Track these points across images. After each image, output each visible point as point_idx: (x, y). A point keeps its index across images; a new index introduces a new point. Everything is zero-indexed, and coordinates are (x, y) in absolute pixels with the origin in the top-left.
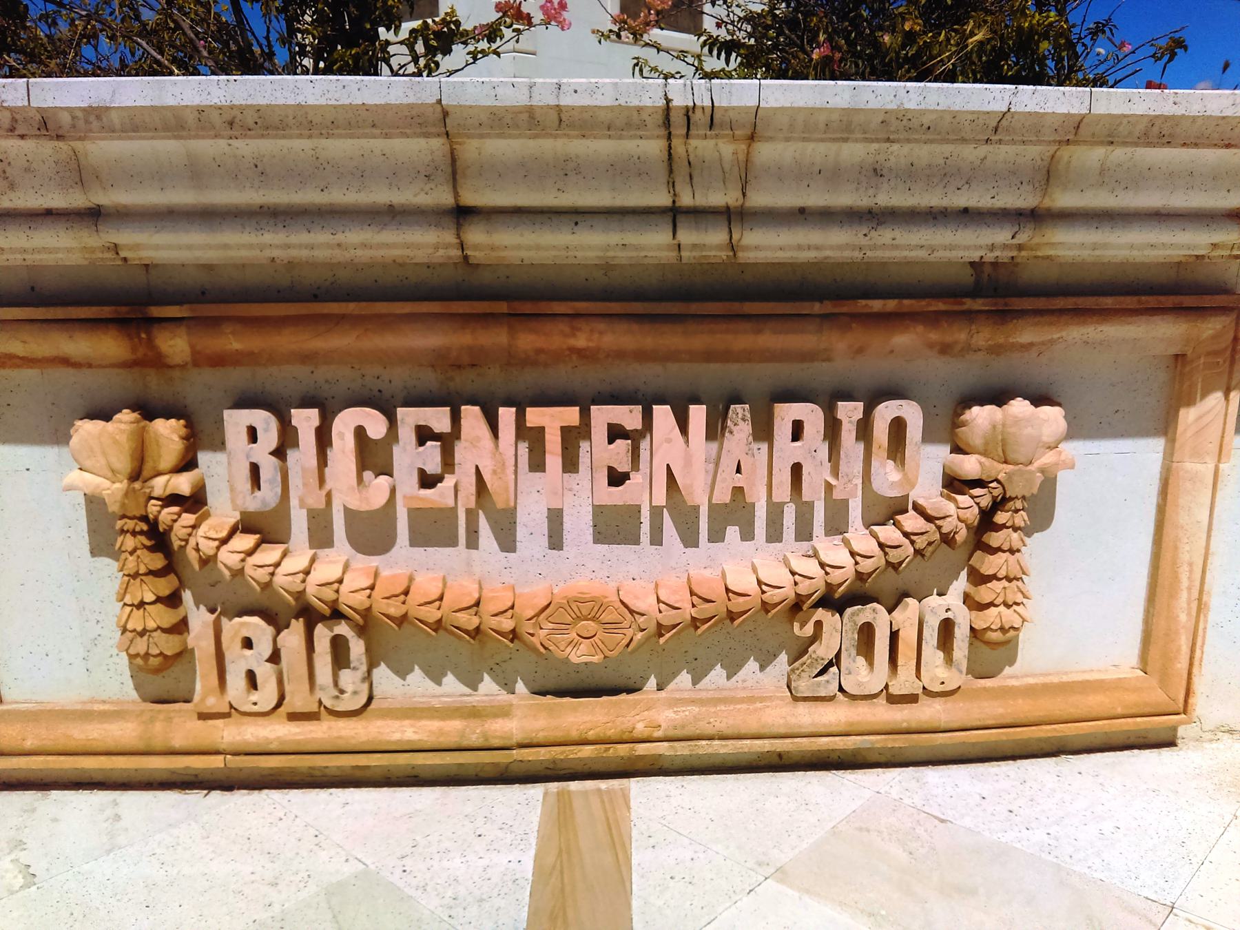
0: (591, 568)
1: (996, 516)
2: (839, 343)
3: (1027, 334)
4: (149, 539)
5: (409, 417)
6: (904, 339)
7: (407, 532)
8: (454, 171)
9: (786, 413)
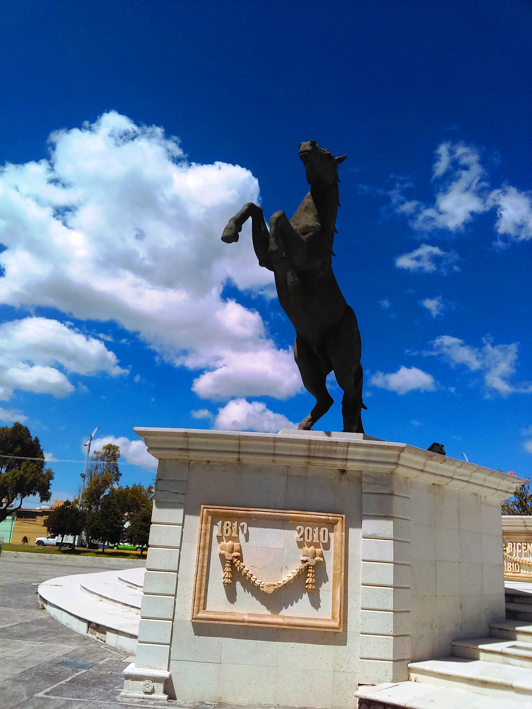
5: (523, 544)
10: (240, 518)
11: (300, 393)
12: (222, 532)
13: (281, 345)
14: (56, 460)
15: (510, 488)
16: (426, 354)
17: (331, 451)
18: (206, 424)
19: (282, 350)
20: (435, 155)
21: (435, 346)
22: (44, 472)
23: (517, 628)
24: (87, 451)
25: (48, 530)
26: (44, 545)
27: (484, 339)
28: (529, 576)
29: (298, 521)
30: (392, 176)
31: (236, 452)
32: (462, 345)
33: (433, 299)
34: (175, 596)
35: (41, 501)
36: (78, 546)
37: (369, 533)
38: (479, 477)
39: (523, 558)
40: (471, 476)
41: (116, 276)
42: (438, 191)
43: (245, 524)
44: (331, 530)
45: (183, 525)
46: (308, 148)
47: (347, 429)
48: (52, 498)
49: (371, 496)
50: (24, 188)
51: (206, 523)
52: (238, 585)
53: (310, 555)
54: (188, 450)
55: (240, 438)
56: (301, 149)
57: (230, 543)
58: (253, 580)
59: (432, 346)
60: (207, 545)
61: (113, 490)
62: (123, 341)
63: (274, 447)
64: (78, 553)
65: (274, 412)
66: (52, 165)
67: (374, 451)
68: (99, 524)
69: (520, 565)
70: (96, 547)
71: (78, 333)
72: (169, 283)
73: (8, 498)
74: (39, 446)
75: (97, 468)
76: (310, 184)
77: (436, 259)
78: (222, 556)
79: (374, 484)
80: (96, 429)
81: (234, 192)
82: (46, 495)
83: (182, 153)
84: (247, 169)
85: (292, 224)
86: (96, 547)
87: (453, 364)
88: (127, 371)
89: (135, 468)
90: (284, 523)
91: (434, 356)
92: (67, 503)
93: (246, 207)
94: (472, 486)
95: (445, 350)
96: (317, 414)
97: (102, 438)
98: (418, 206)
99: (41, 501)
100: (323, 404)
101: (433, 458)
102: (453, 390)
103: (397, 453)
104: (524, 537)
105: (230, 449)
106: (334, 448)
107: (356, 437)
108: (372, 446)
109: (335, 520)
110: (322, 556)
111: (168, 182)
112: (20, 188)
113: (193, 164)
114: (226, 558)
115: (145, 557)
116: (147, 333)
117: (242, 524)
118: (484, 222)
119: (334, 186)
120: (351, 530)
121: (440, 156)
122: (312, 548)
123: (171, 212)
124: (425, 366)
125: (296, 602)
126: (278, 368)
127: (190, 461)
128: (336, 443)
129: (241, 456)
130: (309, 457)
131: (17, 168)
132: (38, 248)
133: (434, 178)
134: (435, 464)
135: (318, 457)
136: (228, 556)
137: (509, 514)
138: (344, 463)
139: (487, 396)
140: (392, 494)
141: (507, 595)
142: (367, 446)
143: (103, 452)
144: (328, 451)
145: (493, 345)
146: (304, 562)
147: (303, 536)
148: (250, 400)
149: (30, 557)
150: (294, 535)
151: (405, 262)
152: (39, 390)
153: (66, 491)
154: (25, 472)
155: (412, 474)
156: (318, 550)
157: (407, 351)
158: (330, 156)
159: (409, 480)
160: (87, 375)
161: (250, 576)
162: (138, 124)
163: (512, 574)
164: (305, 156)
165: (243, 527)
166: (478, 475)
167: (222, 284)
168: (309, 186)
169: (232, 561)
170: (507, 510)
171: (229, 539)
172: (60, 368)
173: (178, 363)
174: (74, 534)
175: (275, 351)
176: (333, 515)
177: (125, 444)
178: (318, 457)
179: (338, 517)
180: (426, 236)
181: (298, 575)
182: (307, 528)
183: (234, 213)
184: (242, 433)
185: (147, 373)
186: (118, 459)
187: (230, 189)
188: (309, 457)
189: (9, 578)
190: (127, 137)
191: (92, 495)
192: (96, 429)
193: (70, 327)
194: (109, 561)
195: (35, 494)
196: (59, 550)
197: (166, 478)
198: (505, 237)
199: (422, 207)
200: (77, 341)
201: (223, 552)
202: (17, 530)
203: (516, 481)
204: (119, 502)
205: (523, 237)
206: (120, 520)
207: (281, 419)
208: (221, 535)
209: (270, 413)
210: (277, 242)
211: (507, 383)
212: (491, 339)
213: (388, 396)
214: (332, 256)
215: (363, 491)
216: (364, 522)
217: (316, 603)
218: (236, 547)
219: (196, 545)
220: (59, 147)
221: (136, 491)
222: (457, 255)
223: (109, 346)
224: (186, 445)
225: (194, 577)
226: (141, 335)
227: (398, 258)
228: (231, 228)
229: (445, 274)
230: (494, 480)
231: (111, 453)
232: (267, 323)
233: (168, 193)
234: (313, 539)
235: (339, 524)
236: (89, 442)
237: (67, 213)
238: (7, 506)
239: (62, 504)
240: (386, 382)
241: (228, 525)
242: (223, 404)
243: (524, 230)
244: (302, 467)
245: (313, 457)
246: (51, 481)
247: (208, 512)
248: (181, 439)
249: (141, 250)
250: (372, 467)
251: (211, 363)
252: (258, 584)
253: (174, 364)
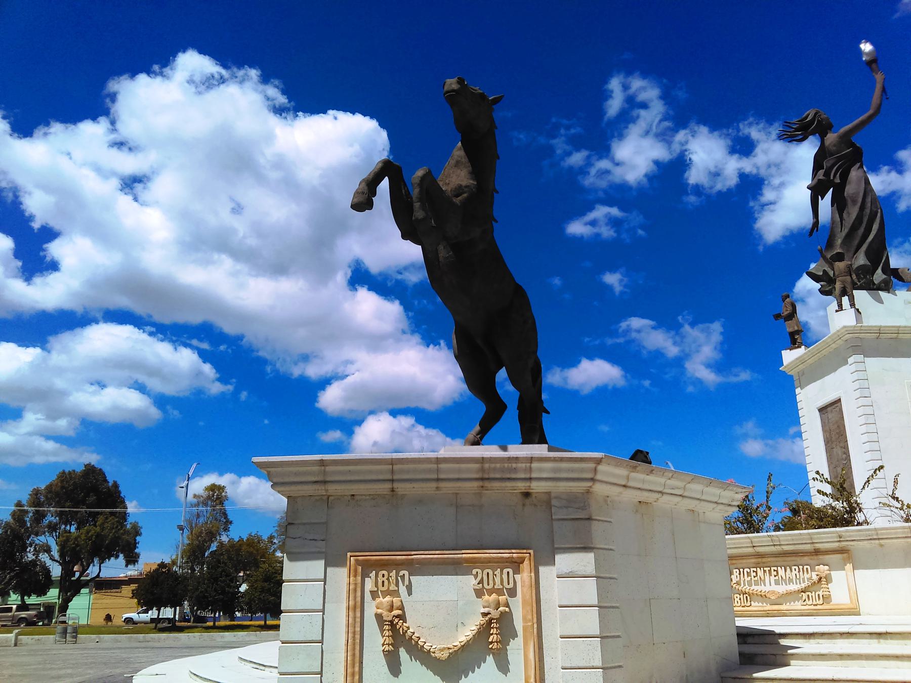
3: (821, 557)
4: (571, 168)
6: (806, 558)
7: (829, 676)
9: (793, 568)
11: (457, 400)
12: (376, 586)
13: (429, 340)
14: (143, 510)
15: (733, 500)
16: (609, 341)
18: (338, 447)
20: (606, 90)
21: (620, 330)
22: (128, 527)
23: (755, 675)
24: (184, 494)
25: (139, 603)
26: (135, 623)
27: (680, 318)
28: (762, 609)
29: (474, 562)
30: (554, 120)
31: (389, 480)
32: (654, 328)
33: (615, 273)
34: (321, 673)
35: (127, 566)
36: (180, 621)
37: (565, 570)
38: (696, 488)
39: (753, 587)
40: (684, 488)
41: (207, 263)
42: (613, 137)
43: (406, 573)
44: (517, 571)
45: (325, 580)
46: (455, 86)
47: (527, 439)
48: (141, 560)
50: (77, 154)
52: (403, 652)
53: (493, 606)
55: (392, 462)
56: (446, 88)
57: (388, 598)
58: (421, 644)
59: (617, 330)
60: (359, 604)
61: (221, 543)
62: (222, 348)
64: (181, 630)
65: (426, 427)
66: (113, 123)
67: (564, 465)
68: (206, 590)
70: (203, 620)
71: (162, 341)
73: (82, 565)
74: (120, 492)
75: (198, 516)
77: (614, 223)
78: (379, 617)
79: (567, 507)
80: (194, 466)
81: (357, 148)
82: (132, 557)
83: (287, 101)
84: (371, 118)
85: (441, 184)
86: (203, 620)
87: (645, 352)
88: (230, 388)
89: (250, 513)
91: (620, 344)
92: (162, 565)
95: (634, 335)
97: (202, 476)
98: (588, 157)
99: (127, 566)
102: (647, 383)
104: (753, 560)
105: (381, 477)
106: (514, 465)
107: (539, 450)
108: (562, 460)
110: (507, 605)
111: (270, 138)
112: (74, 155)
113: (300, 114)
115: (276, 627)
116: (253, 335)
118: (673, 170)
120: (542, 569)
121: (612, 92)
123: (274, 175)
125: (479, 668)
126: (434, 372)
127: (329, 496)
128: (517, 459)
129: (396, 485)
130: (482, 479)
131: (67, 128)
132: (102, 232)
133: (606, 119)
134: (640, 476)
136: (387, 616)
137: (732, 533)
138: (528, 484)
139: (690, 389)
140: (589, 519)
141: (738, 635)
142: (555, 460)
143: (205, 494)
145: (693, 324)
146: (485, 615)
147: (481, 582)
148: (394, 413)
149: (117, 641)
150: (469, 582)
151: (576, 228)
152: (115, 418)
153: (158, 550)
154: (103, 529)
157: (587, 339)
158: (483, 97)
160: (177, 395)
161: (416, 639)
162: (225, 66)
163: (741, 608)
164: (452, 98)
166: (693, 486)
167: (350, 267)
169: (392, 622)
171: (386, 593)
172: (141, 388)
173: (296, 372)
174: (173, 606)
175: (423, 348)
177: (233, 483)
179: (527, 555)
180: (601, 194)
181: (479, 633)
183: (367, 172)
185: (255, 388)
186: (226, 503)
187: (351, 145)
188: (482, 479)
189: (91, 672)
190: (210, 83)
191: (194, 553)
192: (194, 466)
193: (151, 334)
194: (222, 637)
195: (117, 557)
196: (155, 628)
198: (698, 190)
200: (162, 352)
201: (379, 611)
202: (97, 606)
203: (740, 490)
204: (230, 559)
205: (719, 186)
206: (234, 582)
207: (437, 436)
209: (421, 429)
210: (423, 207)
211: (712, 372)
212: (690, 318)
213: (572, 396)
216: (558, 558)
217: (503, 666)
218: (396, 600)
219: (344, 605)
220: (120, 97)
221: (253, 543)
222: (641, 217)
223: (204, 356)
224: (323, 475)
225: (344, 647)
226: (245, 340)
227: (568, 223)
228: (363, 193)
229: (628, 241)
230: (713, 492)
231: (216, 495)
232: (410, 314)
233: (269, 152)
234: (494, 584)
235: (526, 562)
236: (186, 482)
237: (136, 185)
238: (81, 575)
239: (155, 567)
240: (565, 379)
241: (383, 576)
242: (360, 422)
243: (719, 178)
244: (475, 494)
245: (488, 479)
246: (138, 538)
247: (356, 560)
248: (316, 468)
249: (240, 227)
250: (563, 487)
251: (340, 370)
252: (428, 648)
253: (292, 374)
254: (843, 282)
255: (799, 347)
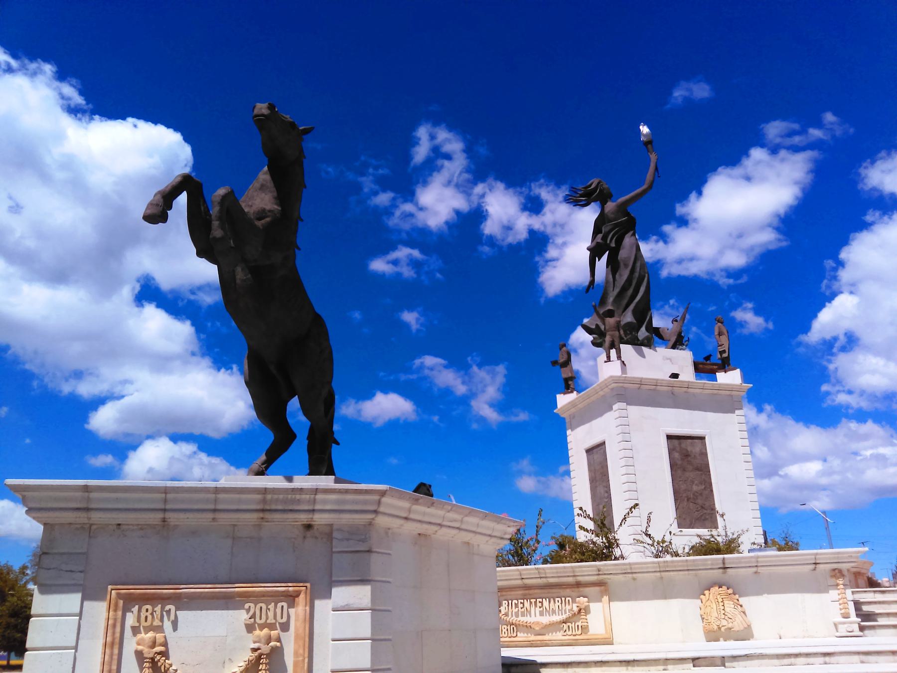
0: (539, 619)
1: (583, 611)
2: (561, 591)
3: (581, 589)
8: (574, 572)
10: (164, 600)
12: (139, 620)
13: (220, 363)
15: (505, 533)
16: (403, 377)
17: (294, 501)
19: (223, 370)
21: (415, 367)
29: (247, 597)
32: (446, 367)
38: (472, 521)
40: (462, 521)
42: (418, 182)
44: (292, 605)
46: (266, 111)
47: (314, 471)
49: (345, 555)
51: (115, 610)
53: (263, 640)
54: (87, 510)
56: (256, 112)
57: (151, 634)
60: (117, 640)
63: (214, 500)
65: (209, 455)
69: (516, 627)
72: (57, 276)
76: (267, 156)
77: (415, 264)
78: (139, 655)
79: (348, 540)
81: (156, 160)
85: (243, 205)
90: (228, 602)
93: (179, 179)
94: (463, 534)
95: (426, 372)
96: (273, 455)
98: (394, 199)
100: (283, 439)
101: (420, 501)
102: (436, 418)
103: (376, 497)
104: (521, 592)
106: (298, 497)
107: (325, 481)
108: (347, 491)
109: (297, 591)
110: (279, 640)
111: (60, 137)
114: (145, 655)
117: (167, 608)
119: (299, 161)
120: (317, 603)
122: (266, 631)
124: (405, 391)
127: (91, 525)
128: (301, 490)
129: (168, 515)
130: (263, 511)
133: (412, 164)
134: (422, 509)
135: (276, 511)
136: (148, 653)
138: (310, 516)
139: (475, 426)
141: (504, 665)
142: (340, 491)
144: (288, 502)
145: (480, 366)
146: (254, 650)
147: (253, 616)
148: (175, 438)
150: (241, 616)
151: (379, 265)
155: (394, 523)
156: (274, 633)
157: (382, 374)
158: (293, 125)
159: (390, 531)
164: (261, 122)
165: (169, 612)
168: (266, 160)
169: (153, 659)
170: (502, 561)
171: (148, 629)
176: (295, 584)
178: (276, 511)
180: (404, 236)
182: (258, 606)
184: (170, 484)
188: (263, 511)
197: (56, 551)
199: (400, 200)
201: (140, 648)
203: (512, 524)
208: (137, 625)
209: (203, 456)
210: (222, 227)
212: (478, 359)
213: (364, 428)
214: (297, 251)
215: (334, 550)
219: (101, 642)
222: (440, 261)
228: (157, 205)
230: (488, 525)
232: (202, 336)
234: (267, 618)
235: (302, 596)
240: (359, 411)
241: (147, 610)
245: (270, 510)
247: (118, 594)
248: (79, 494)
250: (346, 519)
251: (117, 390)
253: (60, 392)
254: (612, 336)
255: (572, 392)
